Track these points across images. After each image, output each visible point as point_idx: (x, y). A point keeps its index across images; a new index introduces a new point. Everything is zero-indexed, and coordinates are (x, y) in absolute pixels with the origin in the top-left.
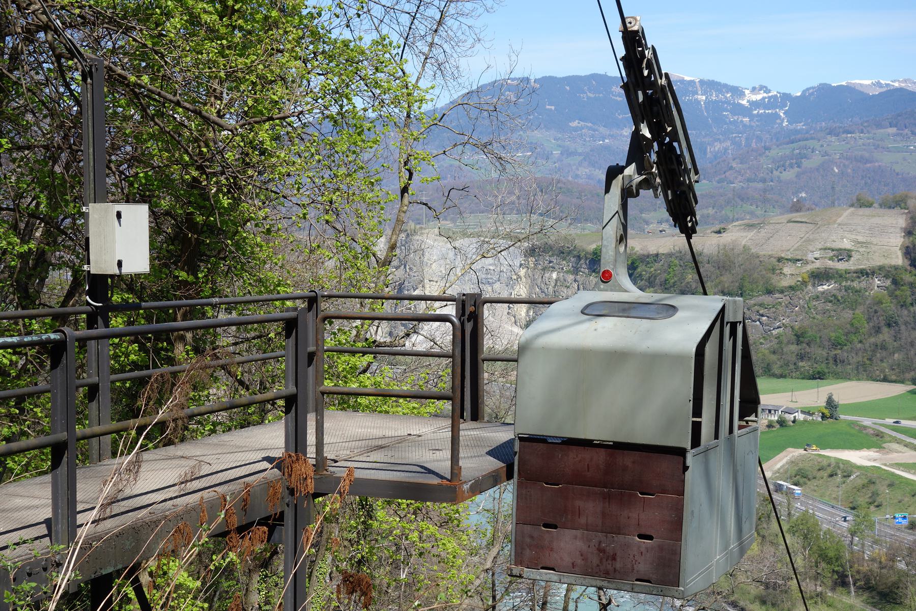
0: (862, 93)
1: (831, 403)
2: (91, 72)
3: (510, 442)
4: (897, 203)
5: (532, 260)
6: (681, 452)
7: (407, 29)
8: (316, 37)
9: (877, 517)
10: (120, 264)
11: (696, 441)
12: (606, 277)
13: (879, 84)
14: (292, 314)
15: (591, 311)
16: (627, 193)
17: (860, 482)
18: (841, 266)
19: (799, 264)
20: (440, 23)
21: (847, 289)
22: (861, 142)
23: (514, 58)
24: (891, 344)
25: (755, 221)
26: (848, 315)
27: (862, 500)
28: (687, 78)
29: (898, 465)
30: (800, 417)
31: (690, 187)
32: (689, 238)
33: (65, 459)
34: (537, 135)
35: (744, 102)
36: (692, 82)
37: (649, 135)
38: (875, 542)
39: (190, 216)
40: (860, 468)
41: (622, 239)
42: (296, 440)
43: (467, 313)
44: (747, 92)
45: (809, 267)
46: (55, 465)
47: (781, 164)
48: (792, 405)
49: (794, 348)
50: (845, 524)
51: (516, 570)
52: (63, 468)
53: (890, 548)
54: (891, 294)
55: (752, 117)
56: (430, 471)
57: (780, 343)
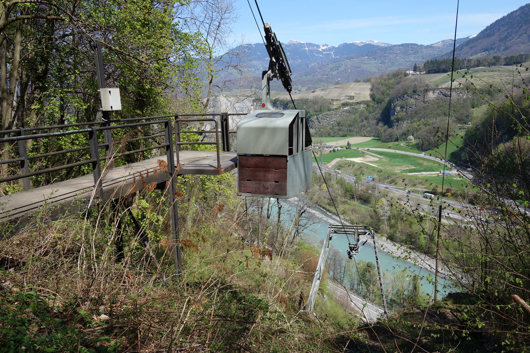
0: (357, 45)
1: (349, 144)
2: (96, 46)
3: (236, 158)
4: (367, 81)
5: (255, 103)
6: (286, 157)
7: (208, 29)
8: (177, 32)
9: (363, 177)
10: (112, 107)
11: (291, 152)
12: (264, 105)
13: (362, 42)
14: (166, 121)
15: (259, 116)
16: (269, 79)
17: (358, 167)
18: (351, 101)
19: (338, 101)
20: (219, 26)
21: (353, 108)
22: (357, 61)
23: (243, 37)
24: (367, 125)
25: (324, 88)
26: (353, 116)
27: (358, 173)
28: (302, 42)
29: (369, 162)
30: (340, 149)
31: (289, 77)
32: (290, 93)
33: (97, 166)
34: (255, 63)
35: (320, 50)
36: (304, 43)
37: (275, 61)
38: (362, 185)
39: (139, 93)
40: (357, 163)
41: (268, 94)
42: (171, 159)
43: (224, 119)
44: (321, 46)
45: (341, 102)
46: (94, 168)
47: (332, 70)
48: (337, 145)
49: (337, 127)
50: (353, 180)
51: (240, 194)
52: (96, 169)
53: (367, 187)
54: (367, 109)
55: (323, 54)
56: (212, 166)
57: (333, 126)
